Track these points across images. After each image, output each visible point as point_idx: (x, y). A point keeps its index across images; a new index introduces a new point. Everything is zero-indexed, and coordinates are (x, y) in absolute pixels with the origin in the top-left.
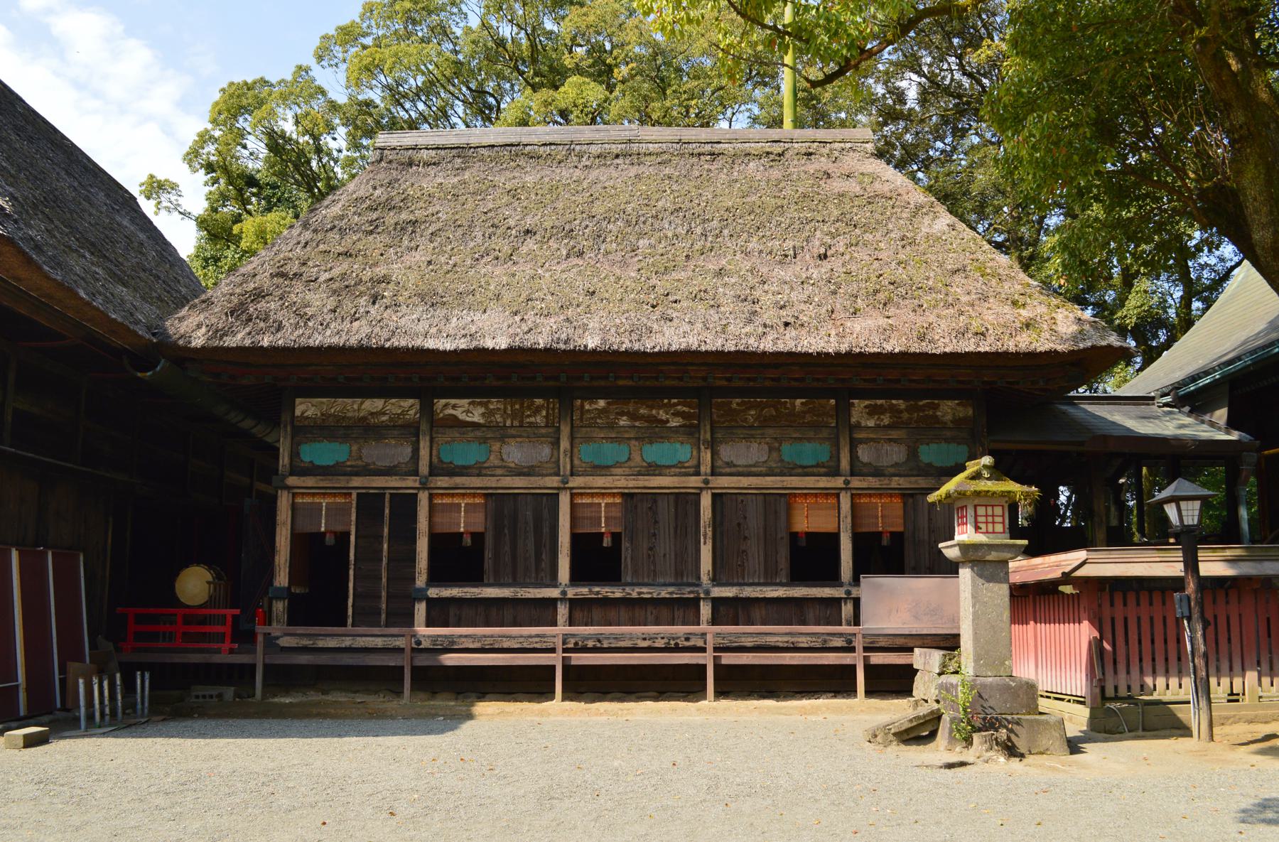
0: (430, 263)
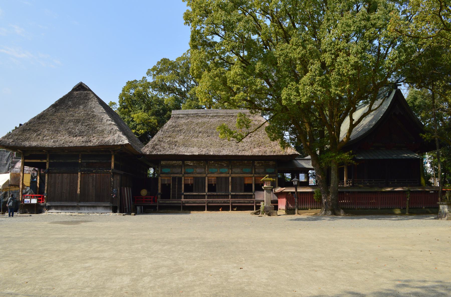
0: (184, 138)
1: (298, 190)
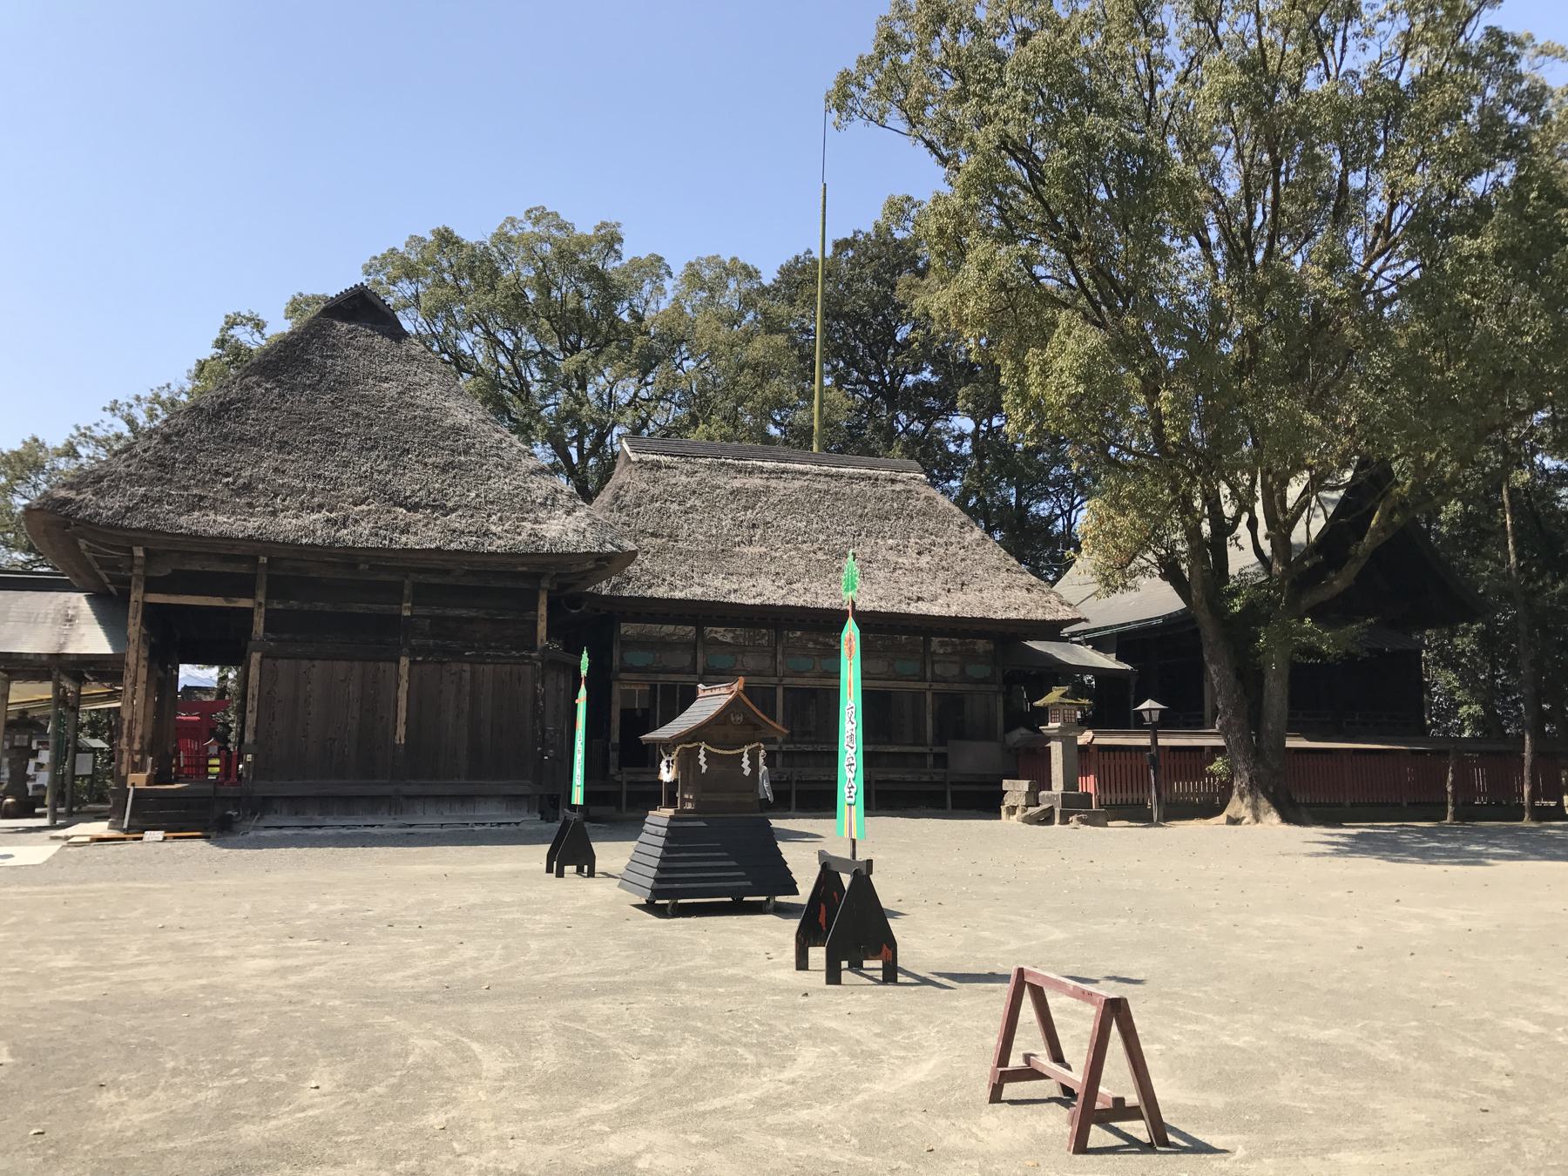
1: (1162, 742)
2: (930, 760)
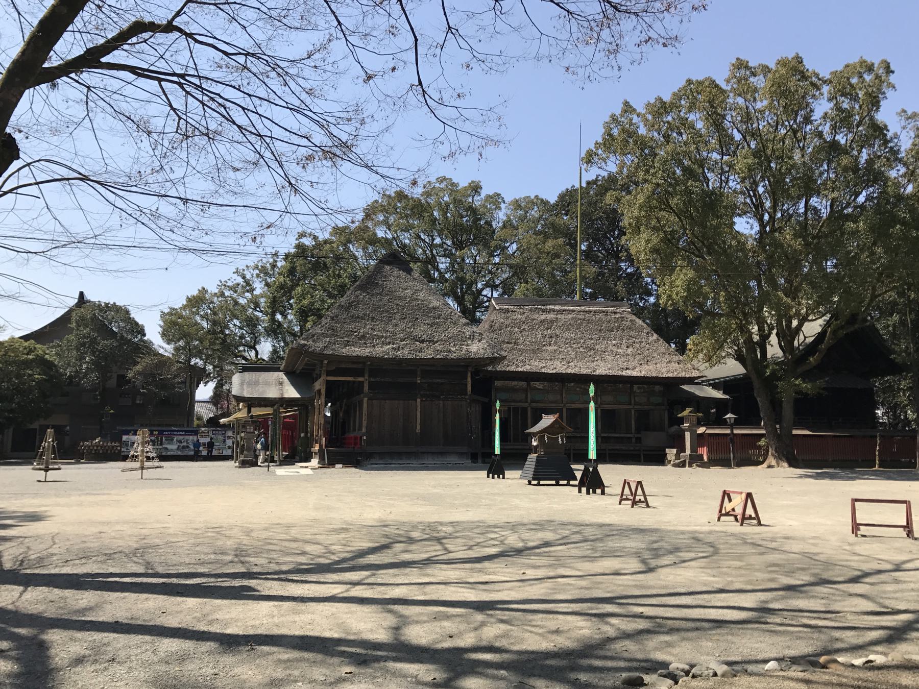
1: (735, 432)
2: (634, 440)
